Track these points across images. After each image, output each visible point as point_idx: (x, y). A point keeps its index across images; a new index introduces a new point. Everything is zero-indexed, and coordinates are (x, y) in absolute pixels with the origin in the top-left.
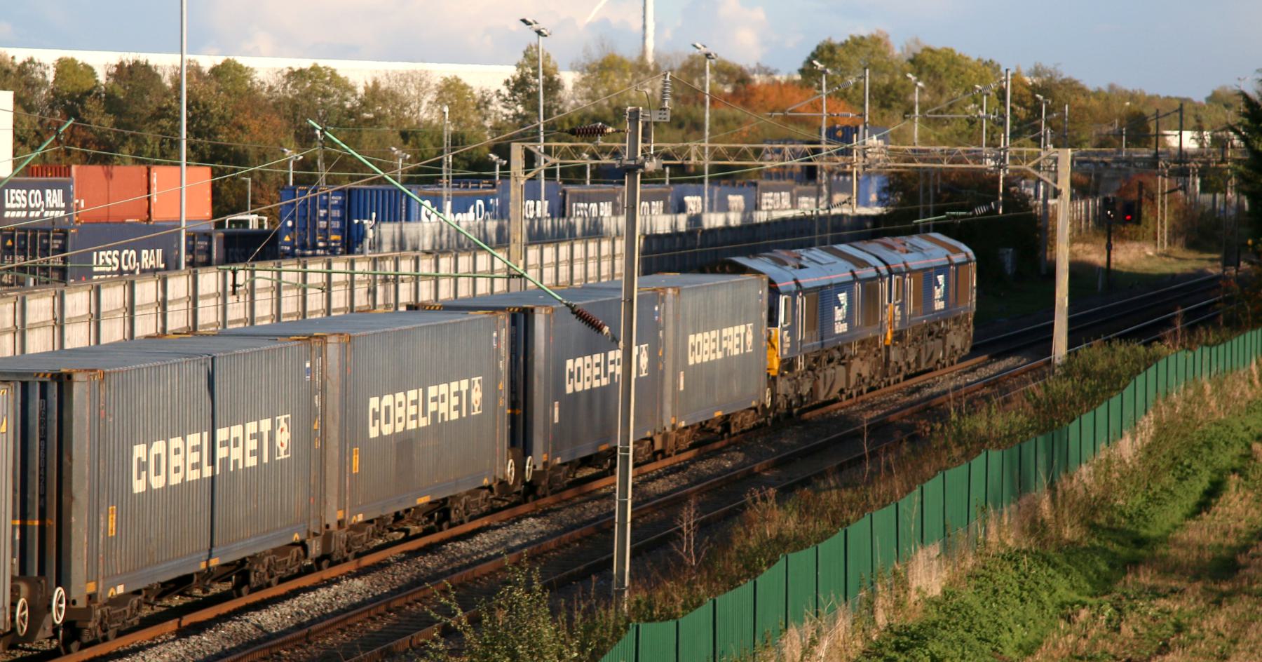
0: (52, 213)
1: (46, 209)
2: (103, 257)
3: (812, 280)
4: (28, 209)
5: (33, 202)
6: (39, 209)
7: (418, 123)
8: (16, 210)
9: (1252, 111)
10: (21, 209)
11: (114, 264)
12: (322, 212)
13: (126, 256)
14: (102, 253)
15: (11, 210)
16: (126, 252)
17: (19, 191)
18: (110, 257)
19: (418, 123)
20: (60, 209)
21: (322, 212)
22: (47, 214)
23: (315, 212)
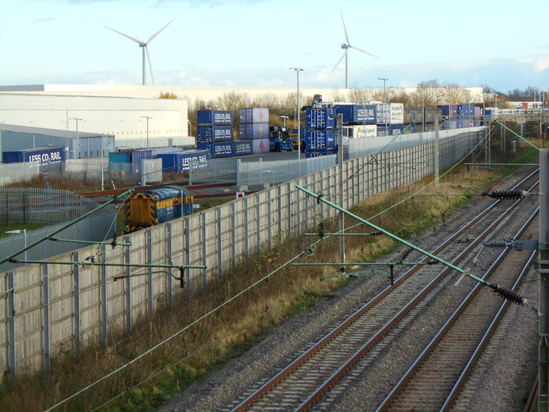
0: (54, 163)
1: (51, 161)
2: (34, 158)
3: (457, 283)
4: (242, 150)
5: (44, 159)
6: (366, 117)
7: (376, 253)
8: (218, 120)
9: (91, 350)
10: (219, 120)
11: (39, 160)
12: (207, 132)
13: (44, 157)
14: (33, 156)
15: (217, 120)
16: (44, 155)
17: (36, 156)
18: (37, 157)
19: (376, 253)
20: (230, 135)
21: (207, 132)
22: (51, 163)
23: (205, 133)
